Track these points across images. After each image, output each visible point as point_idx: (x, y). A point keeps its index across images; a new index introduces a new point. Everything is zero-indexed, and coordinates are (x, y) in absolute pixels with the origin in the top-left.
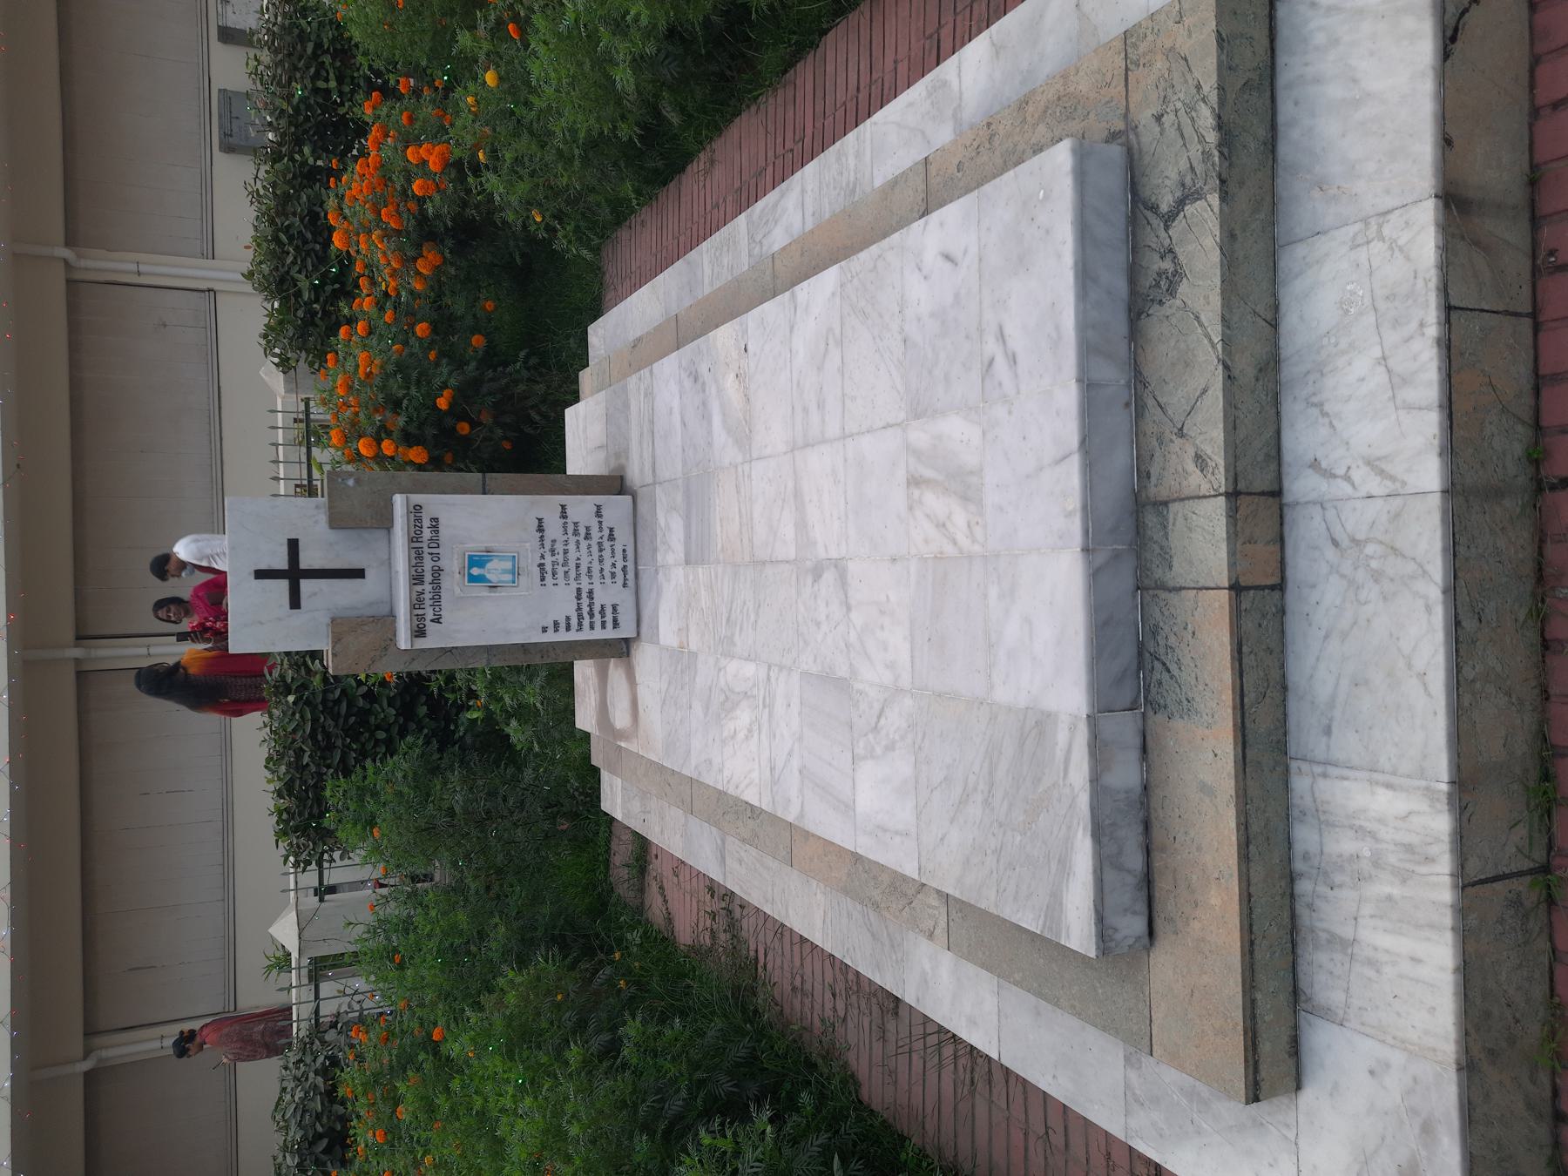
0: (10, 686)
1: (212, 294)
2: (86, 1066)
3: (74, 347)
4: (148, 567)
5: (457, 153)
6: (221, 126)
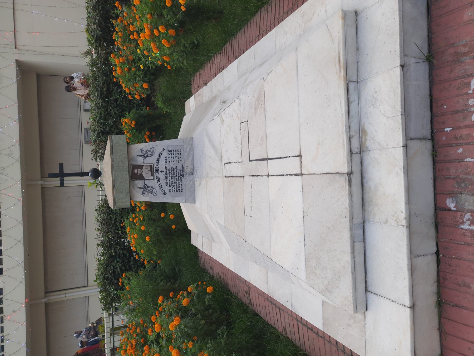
3: (44, 207)
6: (85, 139)
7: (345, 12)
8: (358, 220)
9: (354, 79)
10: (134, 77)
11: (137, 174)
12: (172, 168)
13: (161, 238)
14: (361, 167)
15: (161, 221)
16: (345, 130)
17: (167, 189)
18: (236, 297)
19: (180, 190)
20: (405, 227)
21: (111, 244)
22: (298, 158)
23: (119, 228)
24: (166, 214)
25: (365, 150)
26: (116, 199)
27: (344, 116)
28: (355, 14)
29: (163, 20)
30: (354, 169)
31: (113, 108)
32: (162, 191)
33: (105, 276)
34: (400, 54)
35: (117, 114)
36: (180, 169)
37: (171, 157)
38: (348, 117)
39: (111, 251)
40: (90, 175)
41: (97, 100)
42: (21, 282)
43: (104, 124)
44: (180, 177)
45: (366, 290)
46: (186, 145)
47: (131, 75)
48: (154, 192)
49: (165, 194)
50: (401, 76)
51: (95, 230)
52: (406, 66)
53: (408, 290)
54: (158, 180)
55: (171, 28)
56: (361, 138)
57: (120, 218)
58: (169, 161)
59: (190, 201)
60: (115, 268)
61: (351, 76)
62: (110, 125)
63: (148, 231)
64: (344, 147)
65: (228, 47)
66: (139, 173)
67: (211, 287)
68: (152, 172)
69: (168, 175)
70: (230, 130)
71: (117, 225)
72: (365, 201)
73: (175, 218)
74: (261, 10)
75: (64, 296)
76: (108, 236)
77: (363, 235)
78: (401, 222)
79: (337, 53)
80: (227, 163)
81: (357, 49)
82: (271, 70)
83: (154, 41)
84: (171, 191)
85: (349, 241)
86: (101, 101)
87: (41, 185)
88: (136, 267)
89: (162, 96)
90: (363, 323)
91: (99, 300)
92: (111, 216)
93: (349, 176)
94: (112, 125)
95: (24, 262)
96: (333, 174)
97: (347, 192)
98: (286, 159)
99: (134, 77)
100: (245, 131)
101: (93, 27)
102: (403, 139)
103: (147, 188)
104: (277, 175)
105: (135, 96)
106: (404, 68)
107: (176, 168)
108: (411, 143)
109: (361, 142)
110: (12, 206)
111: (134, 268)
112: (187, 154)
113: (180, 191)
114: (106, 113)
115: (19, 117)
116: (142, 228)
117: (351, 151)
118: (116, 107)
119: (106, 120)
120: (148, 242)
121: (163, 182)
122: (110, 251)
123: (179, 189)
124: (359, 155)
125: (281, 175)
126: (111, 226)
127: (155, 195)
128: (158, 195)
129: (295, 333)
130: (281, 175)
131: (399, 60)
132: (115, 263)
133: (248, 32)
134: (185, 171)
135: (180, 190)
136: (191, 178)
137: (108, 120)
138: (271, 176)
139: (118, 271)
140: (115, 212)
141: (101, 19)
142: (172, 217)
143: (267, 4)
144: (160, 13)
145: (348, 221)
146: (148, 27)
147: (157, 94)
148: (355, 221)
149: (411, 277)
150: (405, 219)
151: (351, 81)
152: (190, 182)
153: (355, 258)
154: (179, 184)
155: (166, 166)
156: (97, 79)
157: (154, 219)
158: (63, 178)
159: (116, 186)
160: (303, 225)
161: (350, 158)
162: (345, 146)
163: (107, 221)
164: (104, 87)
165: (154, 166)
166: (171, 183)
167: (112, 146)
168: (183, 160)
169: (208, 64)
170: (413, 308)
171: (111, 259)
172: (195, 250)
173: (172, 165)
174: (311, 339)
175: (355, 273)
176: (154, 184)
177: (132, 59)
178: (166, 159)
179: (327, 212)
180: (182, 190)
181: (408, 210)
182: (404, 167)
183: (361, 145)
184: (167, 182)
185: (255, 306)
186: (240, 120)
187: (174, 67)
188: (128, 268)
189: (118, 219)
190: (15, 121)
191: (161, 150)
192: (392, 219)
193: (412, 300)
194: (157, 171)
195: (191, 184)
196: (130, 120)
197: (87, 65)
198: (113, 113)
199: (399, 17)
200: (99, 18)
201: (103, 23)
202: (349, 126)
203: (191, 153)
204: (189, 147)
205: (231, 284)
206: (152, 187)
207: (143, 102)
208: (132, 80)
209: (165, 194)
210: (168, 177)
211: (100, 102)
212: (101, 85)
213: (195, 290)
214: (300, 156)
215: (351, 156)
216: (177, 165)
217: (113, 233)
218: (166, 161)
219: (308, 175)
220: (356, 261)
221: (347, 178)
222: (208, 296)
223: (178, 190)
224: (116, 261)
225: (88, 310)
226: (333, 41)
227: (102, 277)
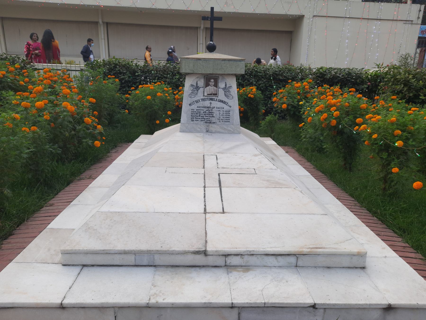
2: (100, 21)
3: (181, 28)
7: (365, 255)
8: (158, 260)
9: (300, 263)
11: (210, 81)
13: (148, 110)
14: (211, 265)
16: (250, 250)
17: (194, 107)
18: (88, 168)
19: (193, 119)
20: (148, 302)
22: (222, 211)
23: (160, 80)
24: (170, 116)
25: (229, 270)
26: (188, 61)
27: (263, 250)
28: (363, 266)
29: (344, 116)
30: (210, 258)
32: (193, 103)
34: (327, 304)
36: (212, 121)
37: (223, 113)
38: (263, 254)
40: (211, 42)
41: (272, 70)
42: (118, 3)
43: (251, 74)
44: (205, 119)
45: (84, 266)
47: (293, 95)
49: (190, 105)
50: (304, 304)
52: (314, 311)
53: (80, 302)
54: (203, 100)
55: (337, 122)
56: (240, 267)
58: (220, 111)
60: (124, 74)
61: (302, 260)
62: (250, 79)
64: (233, 248)
66: (211, 83)
67: (99, 145)
68: (211, 94)
69: (207, 109)
71: (162, 78)
72: (177, 268)
74: (355, 201)
75: (103, 38)
76: (153, 70)
77: (141, 265)
78: (154, 298)
79: (326, 247)
80: (217, 157)
81: (329, 268)
82: (305, 194)
83: (326, 107)
84: (193, 111)
85: (137, 249)
86: (270, 73)
87: (200, 27)
90: (50, 262)
92: (171, 74)
93: (203, 252)
94: (250, 81)
96: (205, 238)
97: (187, 249)
98: (221, 201)
102: (240, 303)
103: (197, 90)
104: (205, 194)
106: (312, 308)
107: (213, 117)
108: (235, 312)
109: (237, 267)
110: (183, 2)
112: (226, 127)
113: (192, 119)
114: (261, 77)
117: (229, 255)
118: (265, 85)
119: (255, 76)
121: (201, 104)
122: (139, 71)
123: (193, 118)
124: (223, 264)
125: (205, 197)
126: (161, 74)
127: (190, 96)
129: (46, 214)
130: (205, 197)
131: (321, 303)
133: (336, 191)
134: (210, 125)
137: (254, 78)
138: (204, 189)
139: (121, 77)
140: (173, 78)
141: (340, 78)
142: (167, 121)
143: (362, 206)
144: (350, 114)
145: (157, 249)
146: (338, 102)
148: (157, 257)
149: (94, 306)
150: (157, 302)
151: (297, 260)
152: (200, 129)
153: (119, 254)
155: (216, 108)
156: (289, 72)
159: (200, 62)
160: (156, 211)
161: (221, 253)
162: (234, 250)
166: (200, 111)
168: (220, 123)
170: (60, 308)
173: (216, 113)
174: (38, 226)
175: (103, 254)
176: (200, 96)
177: (307, 96)
178: (222, 108)
179: (168, 232)
181: (165, 306)
182: (211, 303)
183: (233, 267)
185: (77, 183)
187: (301, 130)
188: (123, 85)
189: (167, 80)
190: (254, 10)
191: (230, 104)
192: (157, 291)
193: (69, 306)
194: (212, 99)
198: (260, 83)
199: (363, 304)
202: (253, 255)
203: (226, 132)
204: (232, 130)
205: (100, 165)
206: (197, 94)
208: (290, 95)
209: (190, 105)
210: (205, 109)
211: (270, 72)
212: (285, 75)
213: (98, 131)
214: (223, 212)
215: (223, 255)
217: (156, 75)
219: (205, 218)
220: (116, 255)
221: (201, 250)
222: (91, 142)
224: (130, 75)
226: (337, 244)
227: (117, 62)
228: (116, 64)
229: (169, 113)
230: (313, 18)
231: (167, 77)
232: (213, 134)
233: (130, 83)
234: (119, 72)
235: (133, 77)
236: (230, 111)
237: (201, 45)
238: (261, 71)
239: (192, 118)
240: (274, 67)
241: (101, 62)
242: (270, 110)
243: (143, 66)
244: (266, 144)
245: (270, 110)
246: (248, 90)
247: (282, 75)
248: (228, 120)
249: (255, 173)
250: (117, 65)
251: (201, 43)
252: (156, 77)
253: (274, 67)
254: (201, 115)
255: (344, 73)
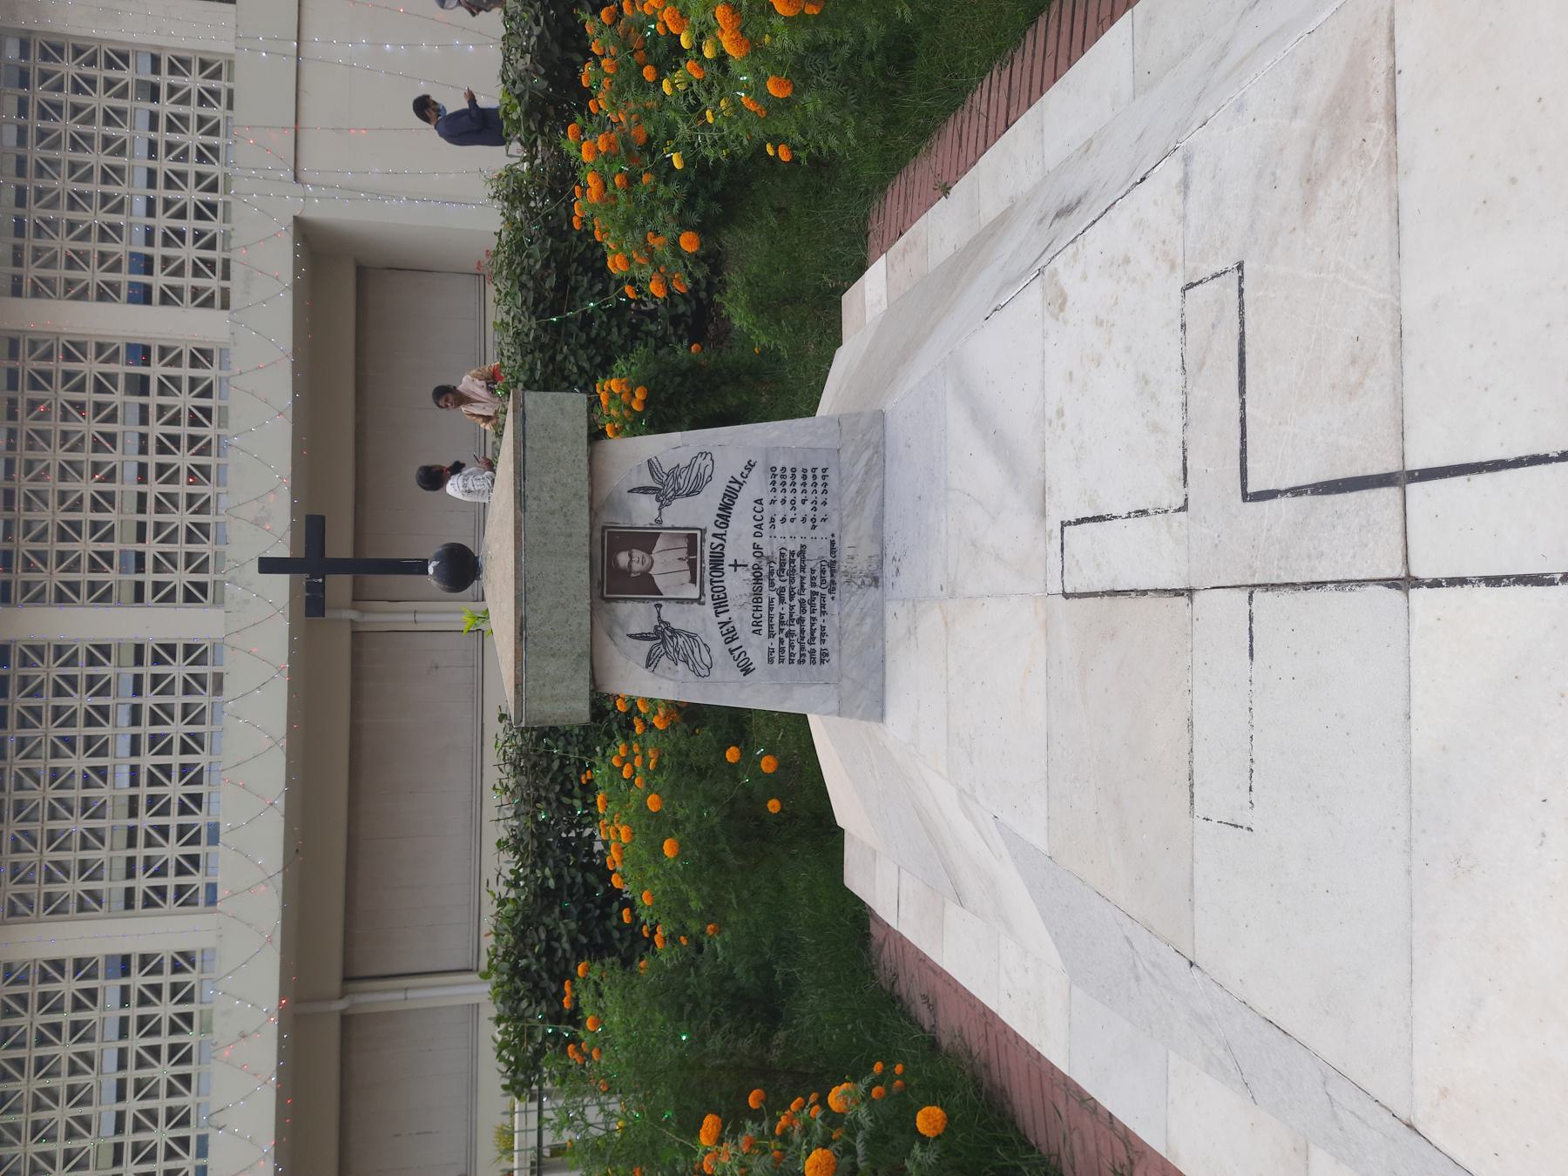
0: (279, 1070)
1: (480, 633)
2: (340, 1005)
3: (360, 366)
4: (414, 481)
5: (730, 294)
10: (648, 208)
11: (627, 572)
12: (783, 551)
13: (724, 850)
15: (727, 777)
17: (756, 647)
19: (818, 655)
21: (544, 844)
23: (573, 787)
24: (747, 752)
31: (573, 352)
32: (736, 653)
33: (516, 963)
35: (586, 372)
37: (784, 501)
39: (543, 873)
40: (431, 570)
41: (520, 321)
42: (270, 940)
44: (817, 593)
46: (852, 449)
48: (698, 659)
49: (747, 670)
51: (494, 788)
54: (720, 604)
57: (581, 753)
58: (773, 520)
59: (858, 707)
60: (552, 936)
63: (675, 814)
65: (1056, 22)
66: (637, 567)
68: (692, 565)
69: (766, 584)
70: (1110, 341)
71: (567, 776)
73: (780, 767)
75: (401, 995)
76: (534, 817)
84: (776, 655)
86: (534, 326)
88: (629, 938)
89: (749, 283)
91: (494, 1049)
92: (550, 743)
95: (281, 875)
99: (648, 208)
100: (1213, 326)
101: (521, 65)
103: (671, 637)
105: (648, 287)
107: (802, 553)
111: (621, 940)
112: (854, 488)
113: (818, 660)
114: (551, 367)
115: (295, 400)
116: (652, 804)
120: (672, 862)
121: (740, 615)
123: (813, 652)
127: (703, 671)
128: (716, 672)
132: (553, 916)
134: (843, 565)
135: (818, 655)
136: (869, 605)
138: (1435, 583)
139: (564, 951)
141: (547, 34)
142: (768, 764)
147: (734, 277)
152: (863, 618)
154: (812, 625)
157: (699, 769)
158: (320, 580)
159: (532, 621)
163: (534, 759)
164: (546, 274)
165: (703, 540)
166: (776, 620)
167: (524, 438)
168: (834, 517)
169: (950, 130)
171: (542, 902)
172: (857, 908)
173: (784, 538)
176: (699, 620)
177: (642, 139)
178: (759, 508)
180: (827, 655)
184: (757, 614)
186: (1179, 273)
187: (803, 155)
188: (600, 940)
189: (571, 756)
190: (280, 414)
191: (737, 470)
194: (717, 561)
195: (866, 628)
196: (627, 384)
197: (494, 197)
198: (575, 370)
200: (542, 33)
201: (556, 50)
205: (1023, 1101)
206: (692, 637)
207: (680, 332)
208: (639, 220)
209: (747, 670)
210: (767, 593)
211: (529, 330)
212: (538, 266)
216: (809, 538)
217: (554, 805)
218: (758, 517)
223: (808, 655)
224: (557, 910)
225: (475, 1051)
227: (506, 966)
228: (511, 969)
229: (732, 754)
230: (304, 184)
231: (561, 758)
232: (890, 552)
233: (589, 911)
234: (544, 959)
235: (565, 898)
236: (773, 469)
237: (419, 617)
238: (527, 367)
239: (813, 662)
240: (508, 313)
241: (506, 1028)
242: (683, 326)
243: (517, 857)
244: (885, 307)
245: (683, 326)
246: (613, 412)
247: (539, 280)
248: (815, 477)
249: (1236, 275)
250: (515, 966)
251: (411, 617)
252: (560, 802)
253: (508, 313)
254: (795, 616)
255: (525, 15)
